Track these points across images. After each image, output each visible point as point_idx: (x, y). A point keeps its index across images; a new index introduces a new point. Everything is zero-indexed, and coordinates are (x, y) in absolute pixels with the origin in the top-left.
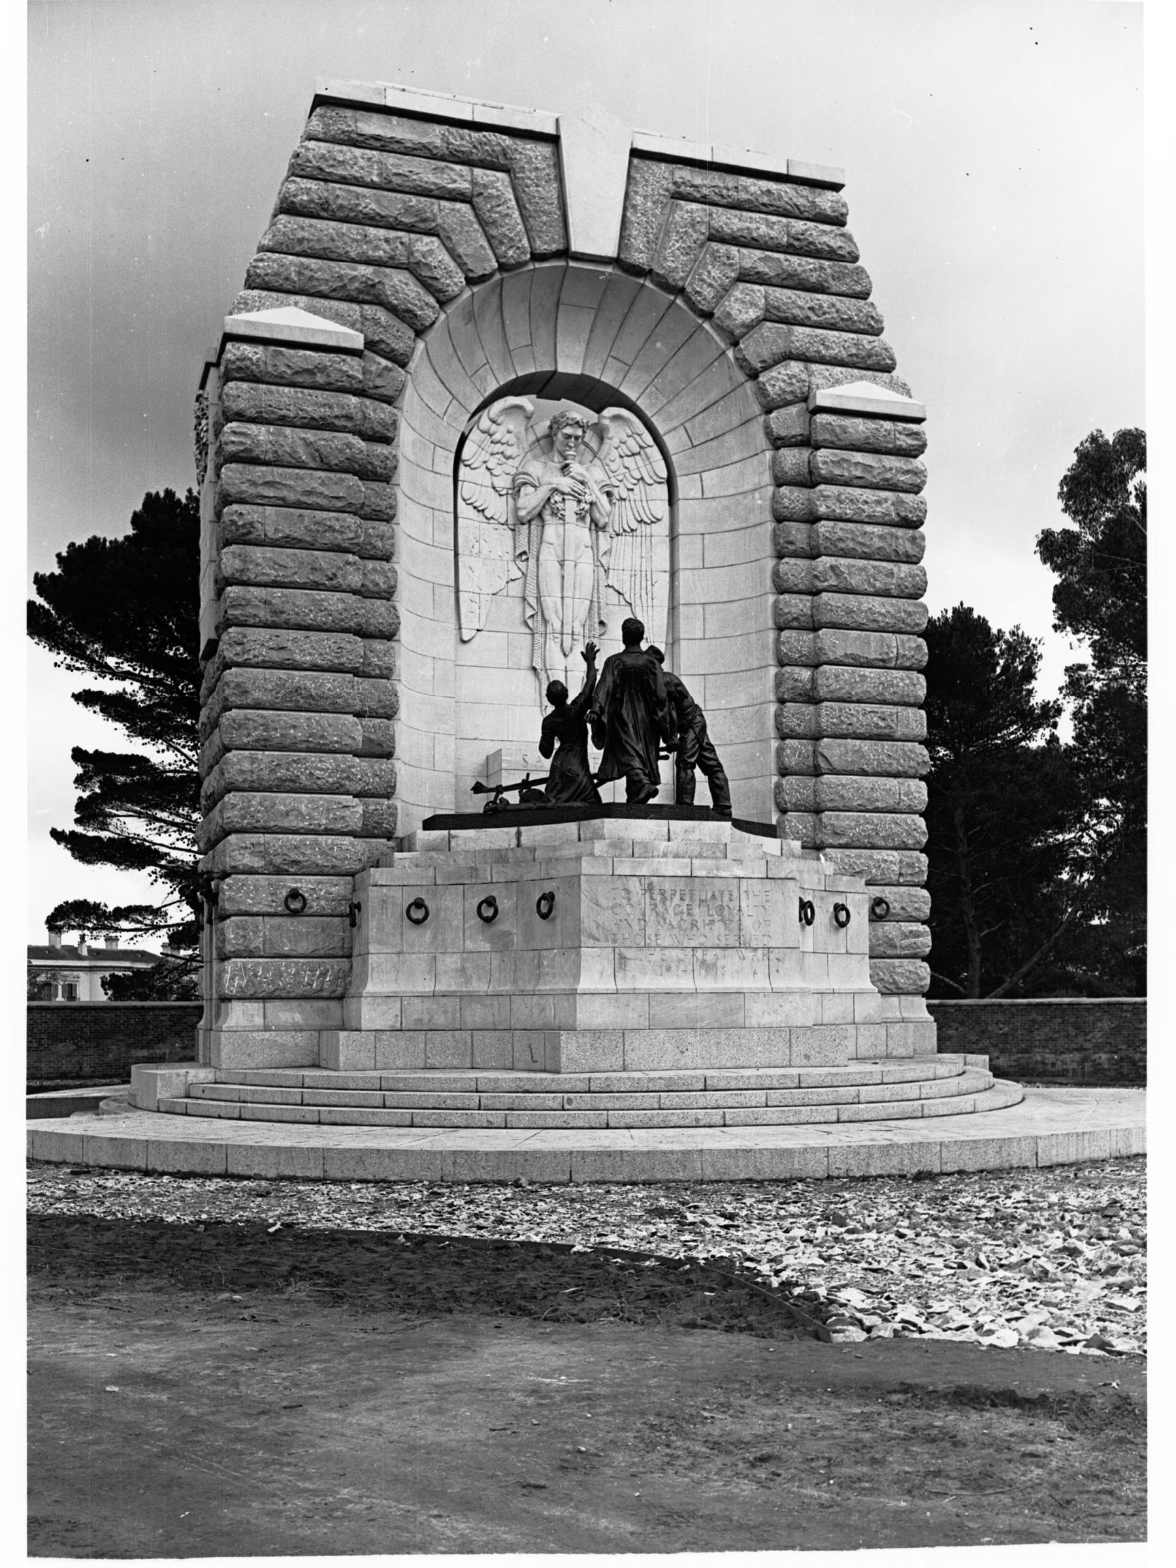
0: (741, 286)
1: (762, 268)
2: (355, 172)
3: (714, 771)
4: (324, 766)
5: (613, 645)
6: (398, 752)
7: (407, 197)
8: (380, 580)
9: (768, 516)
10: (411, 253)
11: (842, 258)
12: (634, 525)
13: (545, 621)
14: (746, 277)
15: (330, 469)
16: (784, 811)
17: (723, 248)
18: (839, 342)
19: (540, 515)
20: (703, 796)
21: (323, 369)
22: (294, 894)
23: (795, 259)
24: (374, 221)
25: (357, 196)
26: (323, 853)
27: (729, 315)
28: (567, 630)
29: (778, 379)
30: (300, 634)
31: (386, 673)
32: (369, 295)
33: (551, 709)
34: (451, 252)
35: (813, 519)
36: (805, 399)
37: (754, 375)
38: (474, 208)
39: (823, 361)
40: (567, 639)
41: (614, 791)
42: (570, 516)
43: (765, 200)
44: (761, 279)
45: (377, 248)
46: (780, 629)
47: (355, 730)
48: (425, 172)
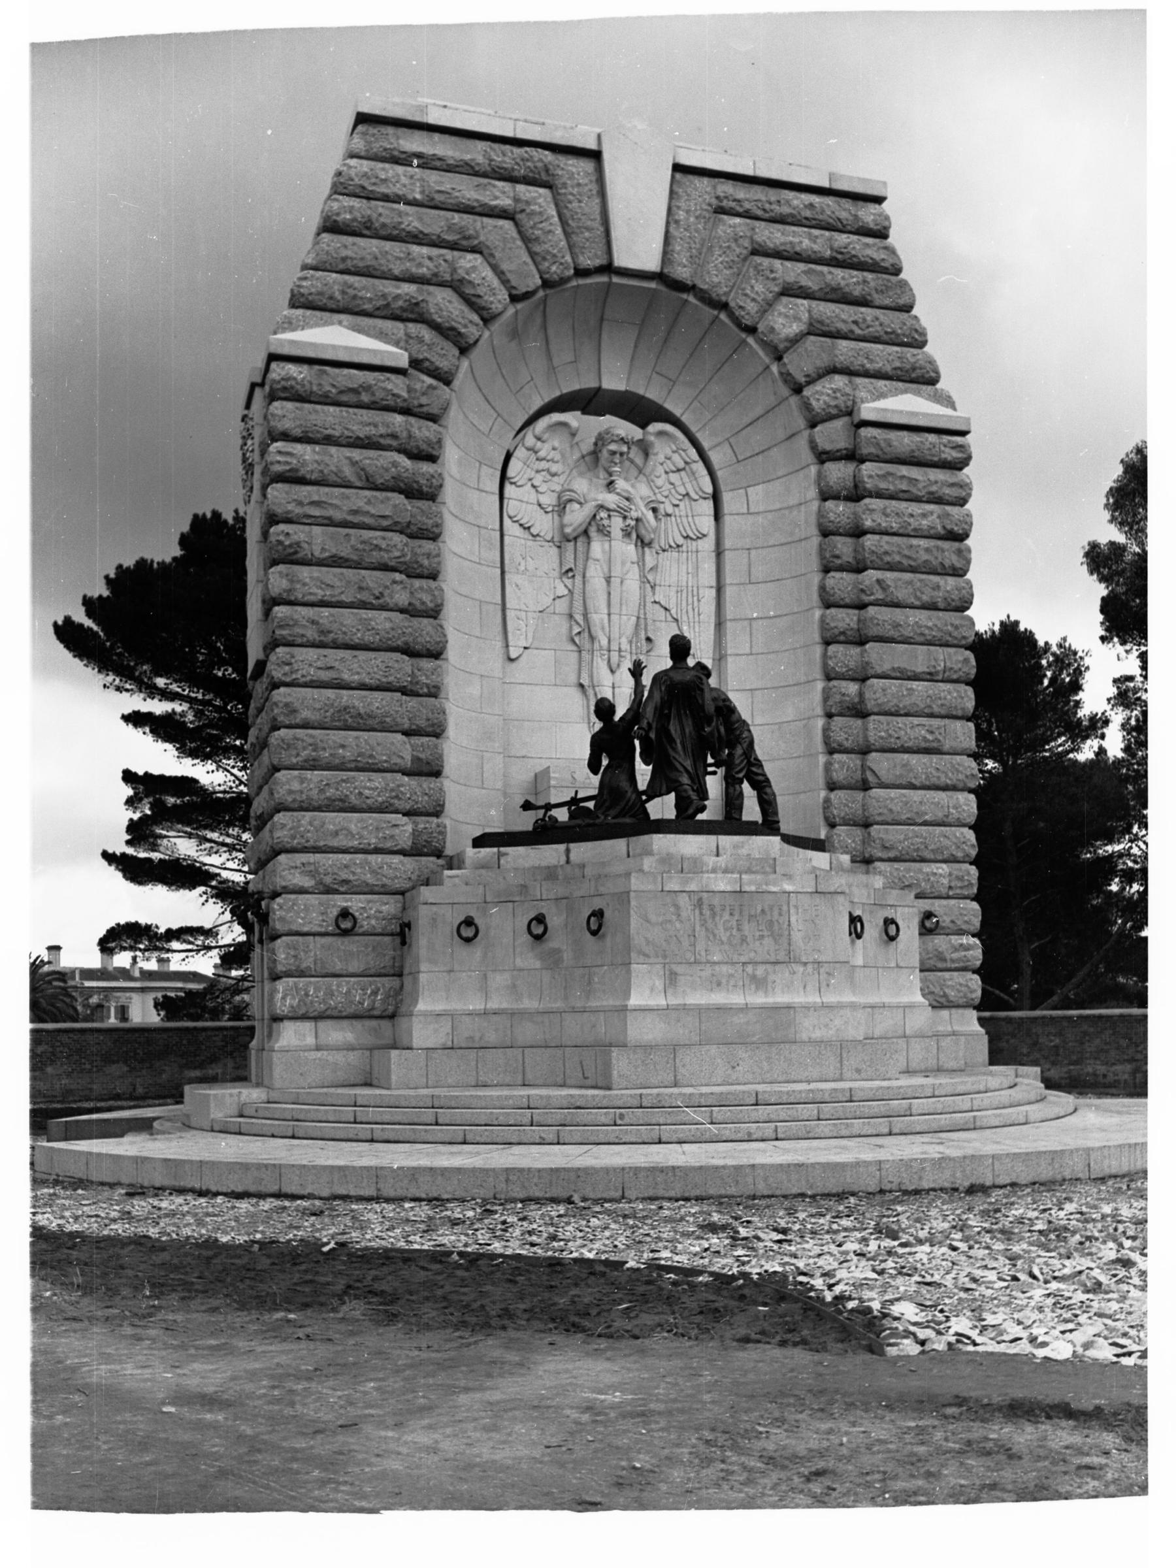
0: (785, 299)
1: (805, 281)
2: (397, 189)
3: (762, 786)
4: (373, 785)
7: (449, 214)
8: (426, 598)
9: (814, 531)
11: (885, 271)
12: (680, 541)
13: (592, 638)
14: (790, 291)
15: (376, 488)
17: (766, 262)
18: (883, 356)
19: (586, 532)
20: (751, 810)
22: (345, 914)
25: (400, 214)
26: (373, 872)
27: (772, 330)
28: (614, 647)
29: (822, 394)
30: (347, 654)
32: (413, 314)
33: (598, 725)
34: (495, 268)
35: (858, 532)
36: (850, 413)
37: (798, 390)
38: (517, 224)
39: (867, 374)
40: (615, 657)
41: (663, 807)
42: (616, 532)
43: (808, 214)
45: (420, 265)
46: (827, 643)
47: (402, 749)
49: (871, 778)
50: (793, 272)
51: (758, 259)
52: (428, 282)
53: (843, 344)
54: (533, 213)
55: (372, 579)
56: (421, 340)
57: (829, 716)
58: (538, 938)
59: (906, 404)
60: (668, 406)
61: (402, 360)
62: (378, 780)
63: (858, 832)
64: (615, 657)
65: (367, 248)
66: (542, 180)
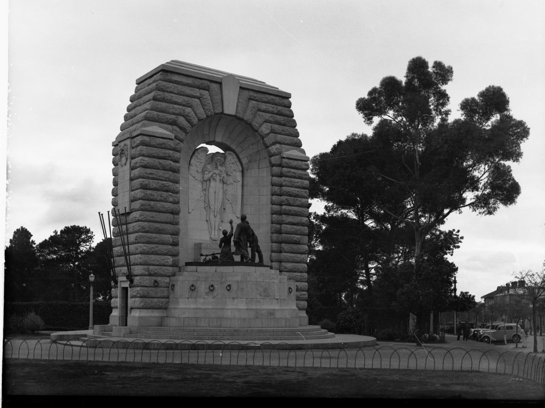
0: (265, 124)
1: (271, 119)
2: (171, 90)
3: (260, 253)
5: (237, 222)
6: (180, 244)
7: (184, 97)
8: (176, 199)
9: (270, 184)
10: (184, 112)
11: (289, 117)
12: (233, 182)
13: (210, 208)
14: (266, 121)
15: (165, 170)
16: (272, 262)
17: (261, 113)
18: (288, 139)
19: (209, 180)
20: (257, 260)
21: (164, 144)
22: (156, 281)
23: (278, 116)
24: (175, 103)
25: (172, 96)
26: (163, 271)
27: (262, 131)
28: (216, 210)
29: (274, 149)
30: (157, 214)
31: (177, 224)
32: (174, 123)
34: (195, 112)
39: (284, 144)
40: (216, 213)
41: (237, 258)
42: (218, 180)
44: (270, 122)
45: (176, 110)
47: (168, 238)
48: (188, 90)
49: (282, 249)
50: (267, 116)
51: (259, 112)
52: (178, 115)
53: (279, 136)
54: (204, 99)
55: (165, 194)
56: (176, 131)
57: (272, 233)
58: (212, 290)
59: (293, 153)
60: (232, 146)
61: (172, 136)
62: (165, 247)
63: (278, 263)
64: (216, 213)
65: (164, 105)
66: (207, 89)
